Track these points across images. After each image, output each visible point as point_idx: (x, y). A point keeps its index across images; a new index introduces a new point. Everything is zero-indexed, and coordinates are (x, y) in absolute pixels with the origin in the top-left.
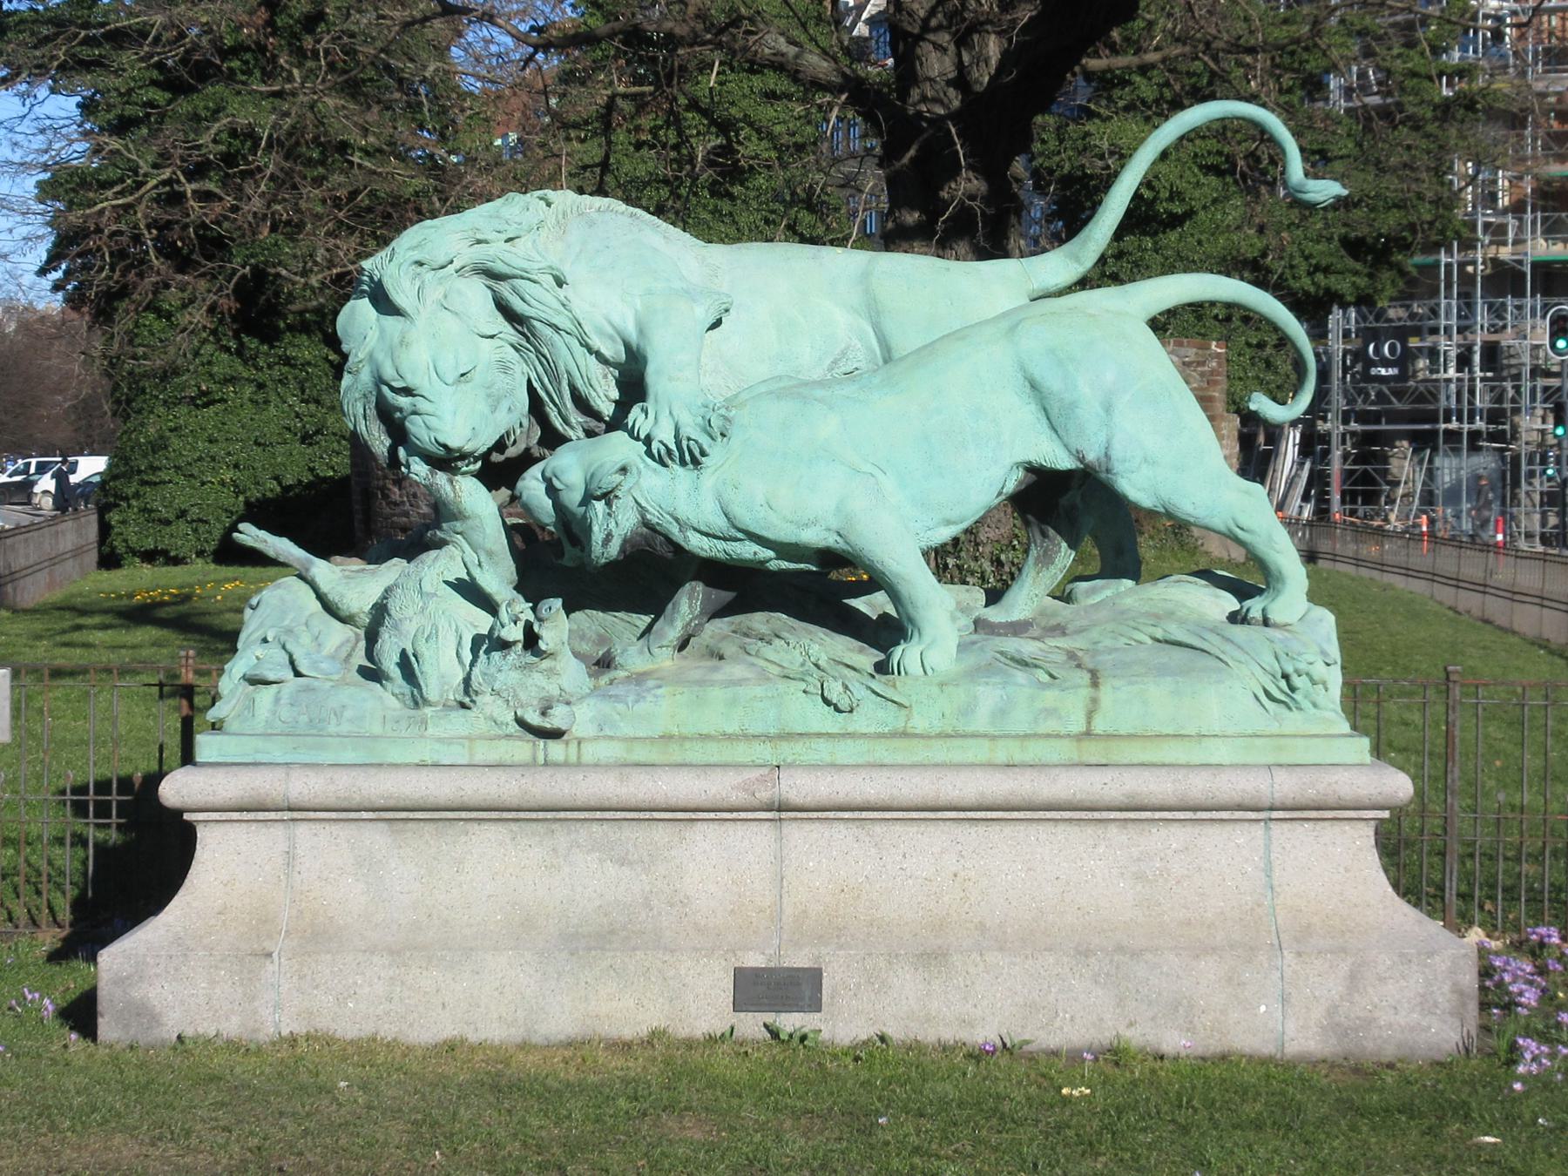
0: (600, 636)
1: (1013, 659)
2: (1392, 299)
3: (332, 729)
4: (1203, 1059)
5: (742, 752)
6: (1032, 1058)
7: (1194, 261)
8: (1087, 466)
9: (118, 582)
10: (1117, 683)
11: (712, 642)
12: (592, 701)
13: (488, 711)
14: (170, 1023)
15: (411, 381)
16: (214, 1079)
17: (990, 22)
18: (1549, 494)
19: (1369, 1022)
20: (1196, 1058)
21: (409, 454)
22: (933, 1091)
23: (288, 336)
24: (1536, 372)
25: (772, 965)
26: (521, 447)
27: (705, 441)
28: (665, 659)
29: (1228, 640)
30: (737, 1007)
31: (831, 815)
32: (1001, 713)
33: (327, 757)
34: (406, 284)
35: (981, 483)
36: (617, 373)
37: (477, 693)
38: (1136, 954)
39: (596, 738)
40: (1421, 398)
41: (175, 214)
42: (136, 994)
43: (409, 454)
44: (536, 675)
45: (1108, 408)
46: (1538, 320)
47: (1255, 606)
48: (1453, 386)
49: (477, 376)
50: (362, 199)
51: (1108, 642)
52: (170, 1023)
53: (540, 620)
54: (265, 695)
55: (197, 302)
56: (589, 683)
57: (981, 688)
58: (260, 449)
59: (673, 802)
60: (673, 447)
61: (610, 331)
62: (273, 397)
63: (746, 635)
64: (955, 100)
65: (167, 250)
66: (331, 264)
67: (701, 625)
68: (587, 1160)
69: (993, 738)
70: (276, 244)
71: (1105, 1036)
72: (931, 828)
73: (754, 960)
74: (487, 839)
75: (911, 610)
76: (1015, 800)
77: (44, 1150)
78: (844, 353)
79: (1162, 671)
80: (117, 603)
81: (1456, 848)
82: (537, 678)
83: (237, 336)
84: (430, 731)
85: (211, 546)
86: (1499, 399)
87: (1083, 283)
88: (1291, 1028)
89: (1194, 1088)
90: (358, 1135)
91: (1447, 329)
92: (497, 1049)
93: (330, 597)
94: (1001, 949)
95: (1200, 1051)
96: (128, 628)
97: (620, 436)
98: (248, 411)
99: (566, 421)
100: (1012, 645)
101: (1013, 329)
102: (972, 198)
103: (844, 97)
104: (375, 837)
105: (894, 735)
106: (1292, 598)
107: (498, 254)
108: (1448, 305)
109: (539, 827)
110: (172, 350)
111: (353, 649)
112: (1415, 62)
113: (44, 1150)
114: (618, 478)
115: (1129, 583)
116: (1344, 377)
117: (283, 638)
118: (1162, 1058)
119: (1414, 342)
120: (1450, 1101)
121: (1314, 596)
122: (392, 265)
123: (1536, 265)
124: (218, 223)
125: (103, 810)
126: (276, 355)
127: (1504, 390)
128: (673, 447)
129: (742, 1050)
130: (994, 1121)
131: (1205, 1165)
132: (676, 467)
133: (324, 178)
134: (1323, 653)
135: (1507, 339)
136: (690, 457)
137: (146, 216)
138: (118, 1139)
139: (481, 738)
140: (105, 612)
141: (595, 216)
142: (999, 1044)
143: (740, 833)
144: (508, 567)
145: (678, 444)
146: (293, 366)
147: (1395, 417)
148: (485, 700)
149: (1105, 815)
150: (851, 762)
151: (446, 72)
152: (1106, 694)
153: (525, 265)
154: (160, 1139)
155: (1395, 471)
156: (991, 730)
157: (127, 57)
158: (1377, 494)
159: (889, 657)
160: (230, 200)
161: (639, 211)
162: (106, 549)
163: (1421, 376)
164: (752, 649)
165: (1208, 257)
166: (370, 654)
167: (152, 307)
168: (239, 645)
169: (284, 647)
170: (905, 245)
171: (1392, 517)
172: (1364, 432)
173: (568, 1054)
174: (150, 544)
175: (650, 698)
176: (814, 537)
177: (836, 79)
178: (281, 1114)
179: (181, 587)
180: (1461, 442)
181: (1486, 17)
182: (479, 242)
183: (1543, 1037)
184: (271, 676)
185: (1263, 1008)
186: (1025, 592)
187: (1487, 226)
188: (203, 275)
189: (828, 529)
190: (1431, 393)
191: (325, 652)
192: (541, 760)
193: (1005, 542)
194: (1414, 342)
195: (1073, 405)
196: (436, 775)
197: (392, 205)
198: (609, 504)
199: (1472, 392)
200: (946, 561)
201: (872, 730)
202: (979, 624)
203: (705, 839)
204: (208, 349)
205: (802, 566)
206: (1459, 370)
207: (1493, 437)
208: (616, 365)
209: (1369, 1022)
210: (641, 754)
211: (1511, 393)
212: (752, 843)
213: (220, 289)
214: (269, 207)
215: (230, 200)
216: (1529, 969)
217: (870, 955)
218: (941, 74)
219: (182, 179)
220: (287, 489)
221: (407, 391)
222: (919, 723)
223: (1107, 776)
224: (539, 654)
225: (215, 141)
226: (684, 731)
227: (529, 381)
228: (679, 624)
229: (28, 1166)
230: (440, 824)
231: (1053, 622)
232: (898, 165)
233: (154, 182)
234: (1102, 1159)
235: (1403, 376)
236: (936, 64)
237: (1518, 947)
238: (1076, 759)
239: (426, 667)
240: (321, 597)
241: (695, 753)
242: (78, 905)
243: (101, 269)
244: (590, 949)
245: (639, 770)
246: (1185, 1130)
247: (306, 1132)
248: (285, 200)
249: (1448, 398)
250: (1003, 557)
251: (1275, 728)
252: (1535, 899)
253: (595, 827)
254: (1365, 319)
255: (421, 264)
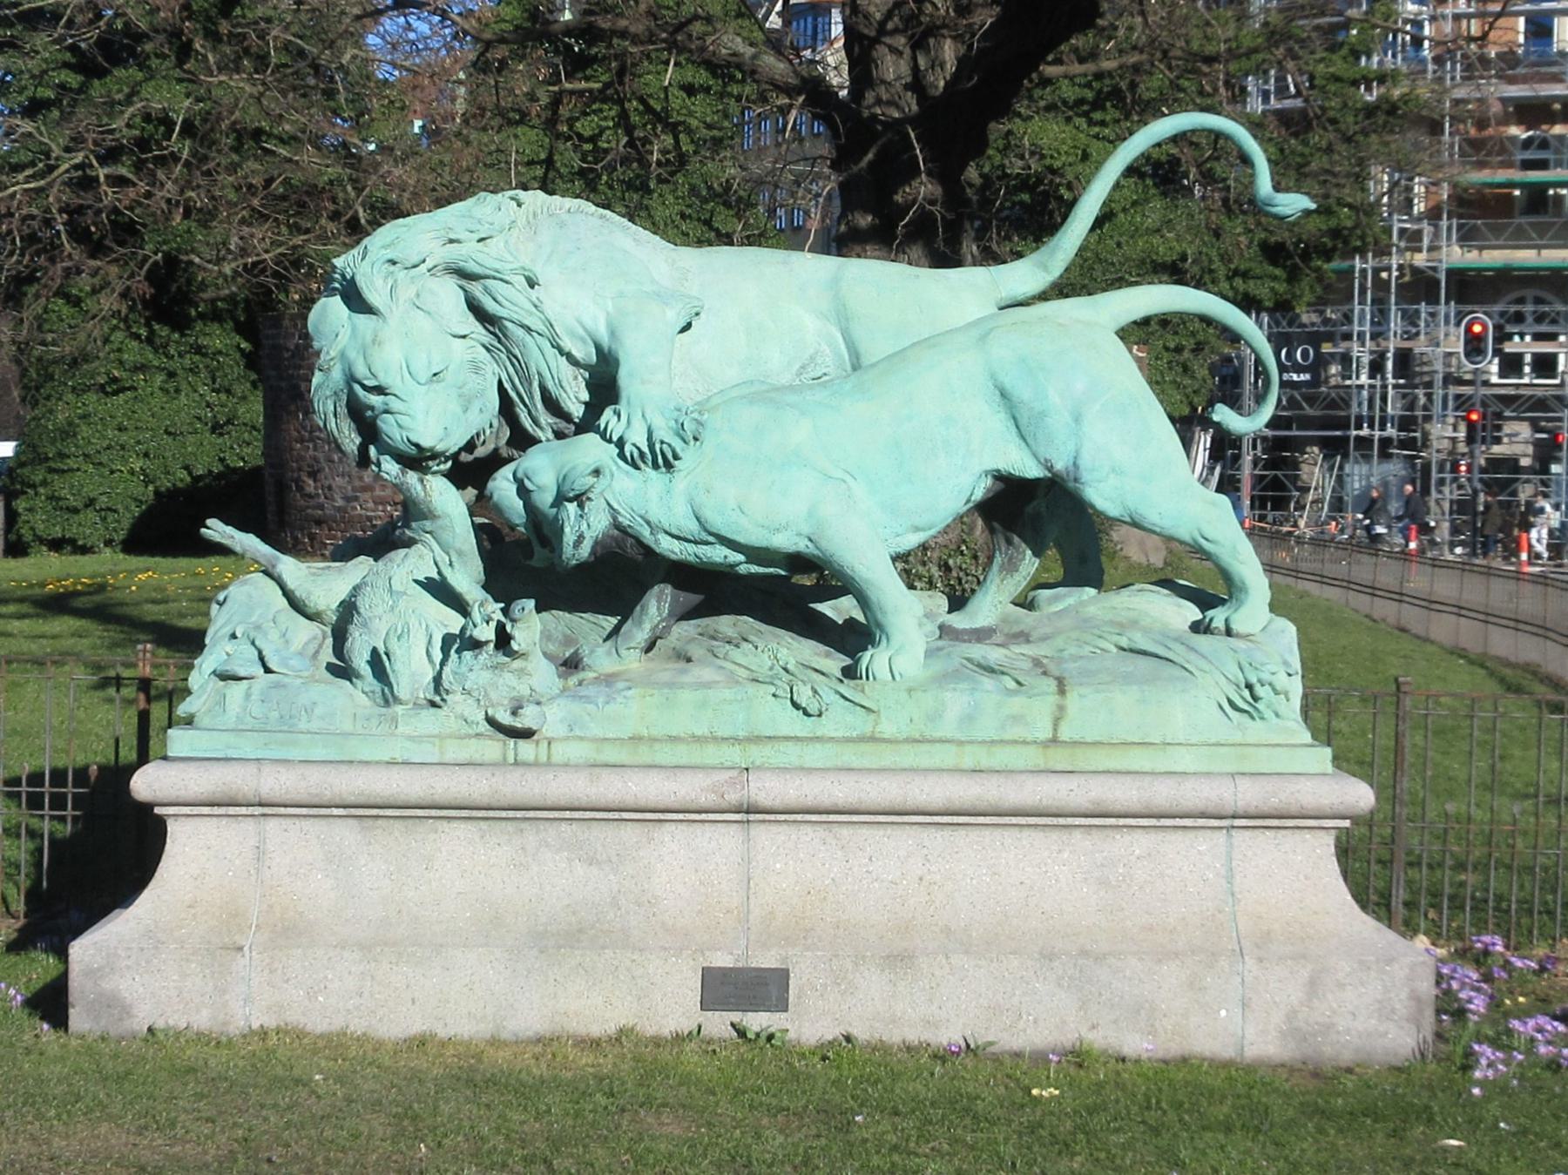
0: (565, 636)
1: (979, 665)
2: (1309, 304)
3: (303, 726)
4: (1166, 1062)
5: (711, 754)
6: (997, 1059)
7: (1113, 264)
8: (1055, 475)
9: (26, 571)
10: (1083, 690)
11: (678, 645)
12: (562, 701)
13: (459, 709)
14: (141, 1015)
15: (384, 380)
16: (192, 1070)
17: (944, 26)
18: (1458, 502)
19: (1330, 1027)
20: (1158, 1061)
21: (380, 452)
22: (905, 1091)
23: (199, 326)
24: (1449, 379)
25: (740, 965)
26: (490, 447)
27: (678, 445)
28: (632, 661)
29: (1192, 649)
30: (704, 1006)
31: (799, 817)
32: (969, 719)
33: (295, 754)
34: (379, 282)
35: (954, 488)
36: (587, 375)
37: (447, 692)
38: (1100, 958)
39: (567, 738)
40: (1333, 405)
41: (87, 199)
42: (107, 985)
43: (380, 452)
44: (507, 675)
45: (1077, 419)
46: (1452, 329)
47: (1218, 616)
48: (1365, 393)
49: (448, 376)
50: (277, 187)
51: (1073, 650)
52: (141, 1015)
53: (513, 621)
54: (236, 690)
55: (109, 287)
56: (558, 683)
57: (948, 695)
58: (170, 440)
59: (642, 803)
60: (646, 450)
61: (581, 331)
62: (184, 386)
63: (714, 638)
64: (911, 104)
65: (79, 234)
66: (243, 252)
67: (667, 629)
68: (572, 1155)
69: (961, 743)
70: (189, 231)
71: (1068, 1039)
72: (898, 831)
73: (722, 960)
74: (457, 837)
75: (879, 616)
76: (982, 806)
77: (33, 1138)
78: (812, 358)
79: (1127, 679)
80: (29, 592)
81: (1402, 857)
82: (508, 678)
83: (148, 325)
84: (400, 729)
85: (121, 535)
86: (1411, 406)
87: (1043, 297)
88: (1251, 1032)
89: (1160, 1090)
90: (342, 1128)
91: (1361, 335)
92: (468, 1044)
93: (297, 594)
94: (967, 952)
95: (1160, 1054)
96: (44, 617)
97: (591, 438)
98: (160, 398)
99: (535, 422)
100: (978, 651)
101: (983, 338)
102: (932, 202)
103: (801, 99)
104: (345, 833)
105: (862, 739)
106: (1253, 609)
107: (470, 254)
108: (1362, 311)
109: (510, 826)
110: (82, 336)
111: (321, 646)
112: (1339, 66)
113: (33, 1138)
114: (591, 480)
115: (1092, 591)
116: (1256, 381)
117: (252, 635)
118: (1124, 1060)
119: (1327, 348)
120: (1413, 1105)
121: (1274, 607)
122: (369, 261)
123: (1451, 273)
124: (131, 209)
125: (58, 802)
126: (186, 343)
127: (1416, 398)
128: (646, 450)
129: (710, 1048)
130: (968, 1121)
131: (1179, 1164)
132: (649, 470)
133: (239, 165)
134: (1286, 663)
135: (1420, 346)
136: (662, 460)
137: (59, 200)
138: (103, 1129)
139: (450, 736)
140: (21, 600)
141: (565, 217)
142: (963, 1045)
143: (708, 835)
144: (477, 565)
145: (651, 446)
146: (205, 355)
147: (1306, 423)
148: (455, 699)
149: (1070, 821)
150: (819, 765)
151: (366, 60)
152: (1072, 700)
153: (497, 265)
154: (146, 1128)
155: (1305, 477)
156: (959, 736)
157: (40, 39)
158: (1288, 499)
159: (857, 662)
160: (143, 187)
161: (607, 212)
162: (12, 537)
163: (1333, 382)
164: (721, 651)
165: (1128, 259)
166: (339, 650)
167: (61, 293)
168: (207, 641)
169: (253, 643)
170: (858, 249)
171: (1302, 523)
172: (1275, 437)
173: (538, 1049)
174: (57, 532)
175: (620, 700)
176: (786, 541)
177: (793, 81)
178: (262, 1106)
179: (91, 577)
180: (1372, 449)
181: (1406, 21)
182: (451, 241)
183: (1495, 1043)
184: (242, 673)
185: (1223, 1013)
186: (989, 598)
187: (1402, 232)
188: (116, 260)
189: (799, 534)
190: (1342, 399)
191: (292, 649)
192: (544, 759)
193: (954, 547)
194: (1327, 348)
195: (1043, 415)
196: (406, 773)
197: (308, 193)
198: (581, 506)
199: (1384, 399)
200: (912, 567)
201: (839, 734)
202: (944, 630)
203: (673, 840)
204: (118, 336)
205: (771, 570)
206: (1372, 376)
207: (1403, 444)
208: (586, 367)
209: (1330, 1027)
210: (612, 754)
211: (1422, 400)
212: (720, 844)
213: (132, 276)
214: (182, 192)
215: (143, 187)
216: (1475, 976)
217: (836, 956)
218: (899, 78)
219: (95, 162)
220: (200, 478)
221: (380, 390)
222: (887, 729)
223: (1073, 782)
224: (511, 654)
225: (128, 126)
226: (655, 732)
227: (500, 383)
228: (647, 626)
229: (19, 1153)
230: (411, 821)
231: (1016, 629)
232: (855, 169)
233: (66, 166)
234: (1079, 1158)
235: (1315, 382)
236: (892, 67)
237: (1462, 954)
238: (1042, 767)
239: (398, 666)
240: (288, 594)
241: (665, 755)
242: (33, 896)
243: (12, 254)
244: (560, 947)
245: (609, 770)
246: (1156, 1131)
247: (288, 1124)
248: (199, 186)
249: (1360, 404)
250: (951, 562)
251: (1238, 737)
252: (1479, 906)
253: (564, 826)
254: (1278, 324)
255: (394, 263)
